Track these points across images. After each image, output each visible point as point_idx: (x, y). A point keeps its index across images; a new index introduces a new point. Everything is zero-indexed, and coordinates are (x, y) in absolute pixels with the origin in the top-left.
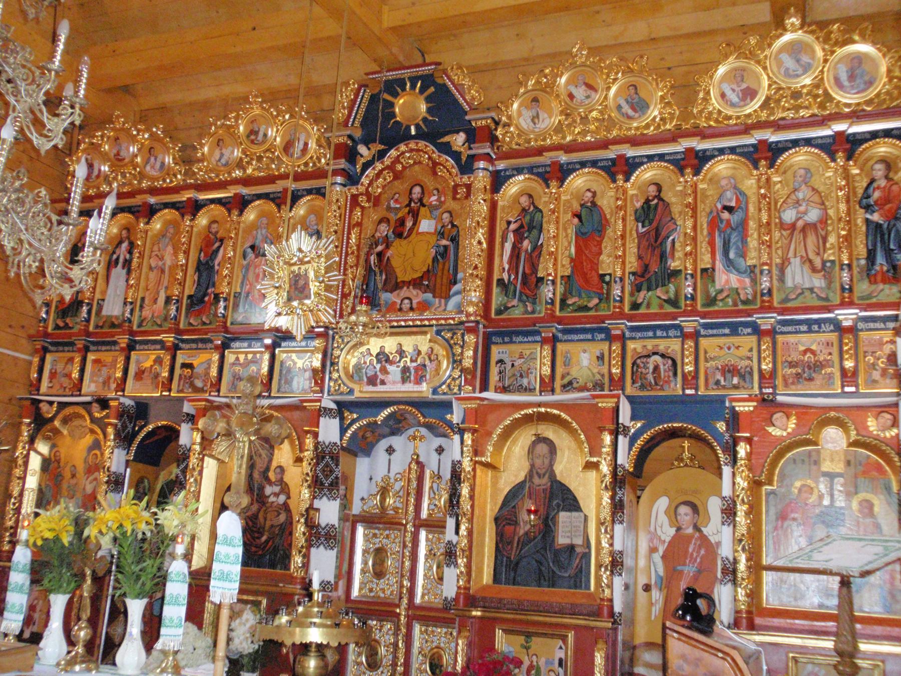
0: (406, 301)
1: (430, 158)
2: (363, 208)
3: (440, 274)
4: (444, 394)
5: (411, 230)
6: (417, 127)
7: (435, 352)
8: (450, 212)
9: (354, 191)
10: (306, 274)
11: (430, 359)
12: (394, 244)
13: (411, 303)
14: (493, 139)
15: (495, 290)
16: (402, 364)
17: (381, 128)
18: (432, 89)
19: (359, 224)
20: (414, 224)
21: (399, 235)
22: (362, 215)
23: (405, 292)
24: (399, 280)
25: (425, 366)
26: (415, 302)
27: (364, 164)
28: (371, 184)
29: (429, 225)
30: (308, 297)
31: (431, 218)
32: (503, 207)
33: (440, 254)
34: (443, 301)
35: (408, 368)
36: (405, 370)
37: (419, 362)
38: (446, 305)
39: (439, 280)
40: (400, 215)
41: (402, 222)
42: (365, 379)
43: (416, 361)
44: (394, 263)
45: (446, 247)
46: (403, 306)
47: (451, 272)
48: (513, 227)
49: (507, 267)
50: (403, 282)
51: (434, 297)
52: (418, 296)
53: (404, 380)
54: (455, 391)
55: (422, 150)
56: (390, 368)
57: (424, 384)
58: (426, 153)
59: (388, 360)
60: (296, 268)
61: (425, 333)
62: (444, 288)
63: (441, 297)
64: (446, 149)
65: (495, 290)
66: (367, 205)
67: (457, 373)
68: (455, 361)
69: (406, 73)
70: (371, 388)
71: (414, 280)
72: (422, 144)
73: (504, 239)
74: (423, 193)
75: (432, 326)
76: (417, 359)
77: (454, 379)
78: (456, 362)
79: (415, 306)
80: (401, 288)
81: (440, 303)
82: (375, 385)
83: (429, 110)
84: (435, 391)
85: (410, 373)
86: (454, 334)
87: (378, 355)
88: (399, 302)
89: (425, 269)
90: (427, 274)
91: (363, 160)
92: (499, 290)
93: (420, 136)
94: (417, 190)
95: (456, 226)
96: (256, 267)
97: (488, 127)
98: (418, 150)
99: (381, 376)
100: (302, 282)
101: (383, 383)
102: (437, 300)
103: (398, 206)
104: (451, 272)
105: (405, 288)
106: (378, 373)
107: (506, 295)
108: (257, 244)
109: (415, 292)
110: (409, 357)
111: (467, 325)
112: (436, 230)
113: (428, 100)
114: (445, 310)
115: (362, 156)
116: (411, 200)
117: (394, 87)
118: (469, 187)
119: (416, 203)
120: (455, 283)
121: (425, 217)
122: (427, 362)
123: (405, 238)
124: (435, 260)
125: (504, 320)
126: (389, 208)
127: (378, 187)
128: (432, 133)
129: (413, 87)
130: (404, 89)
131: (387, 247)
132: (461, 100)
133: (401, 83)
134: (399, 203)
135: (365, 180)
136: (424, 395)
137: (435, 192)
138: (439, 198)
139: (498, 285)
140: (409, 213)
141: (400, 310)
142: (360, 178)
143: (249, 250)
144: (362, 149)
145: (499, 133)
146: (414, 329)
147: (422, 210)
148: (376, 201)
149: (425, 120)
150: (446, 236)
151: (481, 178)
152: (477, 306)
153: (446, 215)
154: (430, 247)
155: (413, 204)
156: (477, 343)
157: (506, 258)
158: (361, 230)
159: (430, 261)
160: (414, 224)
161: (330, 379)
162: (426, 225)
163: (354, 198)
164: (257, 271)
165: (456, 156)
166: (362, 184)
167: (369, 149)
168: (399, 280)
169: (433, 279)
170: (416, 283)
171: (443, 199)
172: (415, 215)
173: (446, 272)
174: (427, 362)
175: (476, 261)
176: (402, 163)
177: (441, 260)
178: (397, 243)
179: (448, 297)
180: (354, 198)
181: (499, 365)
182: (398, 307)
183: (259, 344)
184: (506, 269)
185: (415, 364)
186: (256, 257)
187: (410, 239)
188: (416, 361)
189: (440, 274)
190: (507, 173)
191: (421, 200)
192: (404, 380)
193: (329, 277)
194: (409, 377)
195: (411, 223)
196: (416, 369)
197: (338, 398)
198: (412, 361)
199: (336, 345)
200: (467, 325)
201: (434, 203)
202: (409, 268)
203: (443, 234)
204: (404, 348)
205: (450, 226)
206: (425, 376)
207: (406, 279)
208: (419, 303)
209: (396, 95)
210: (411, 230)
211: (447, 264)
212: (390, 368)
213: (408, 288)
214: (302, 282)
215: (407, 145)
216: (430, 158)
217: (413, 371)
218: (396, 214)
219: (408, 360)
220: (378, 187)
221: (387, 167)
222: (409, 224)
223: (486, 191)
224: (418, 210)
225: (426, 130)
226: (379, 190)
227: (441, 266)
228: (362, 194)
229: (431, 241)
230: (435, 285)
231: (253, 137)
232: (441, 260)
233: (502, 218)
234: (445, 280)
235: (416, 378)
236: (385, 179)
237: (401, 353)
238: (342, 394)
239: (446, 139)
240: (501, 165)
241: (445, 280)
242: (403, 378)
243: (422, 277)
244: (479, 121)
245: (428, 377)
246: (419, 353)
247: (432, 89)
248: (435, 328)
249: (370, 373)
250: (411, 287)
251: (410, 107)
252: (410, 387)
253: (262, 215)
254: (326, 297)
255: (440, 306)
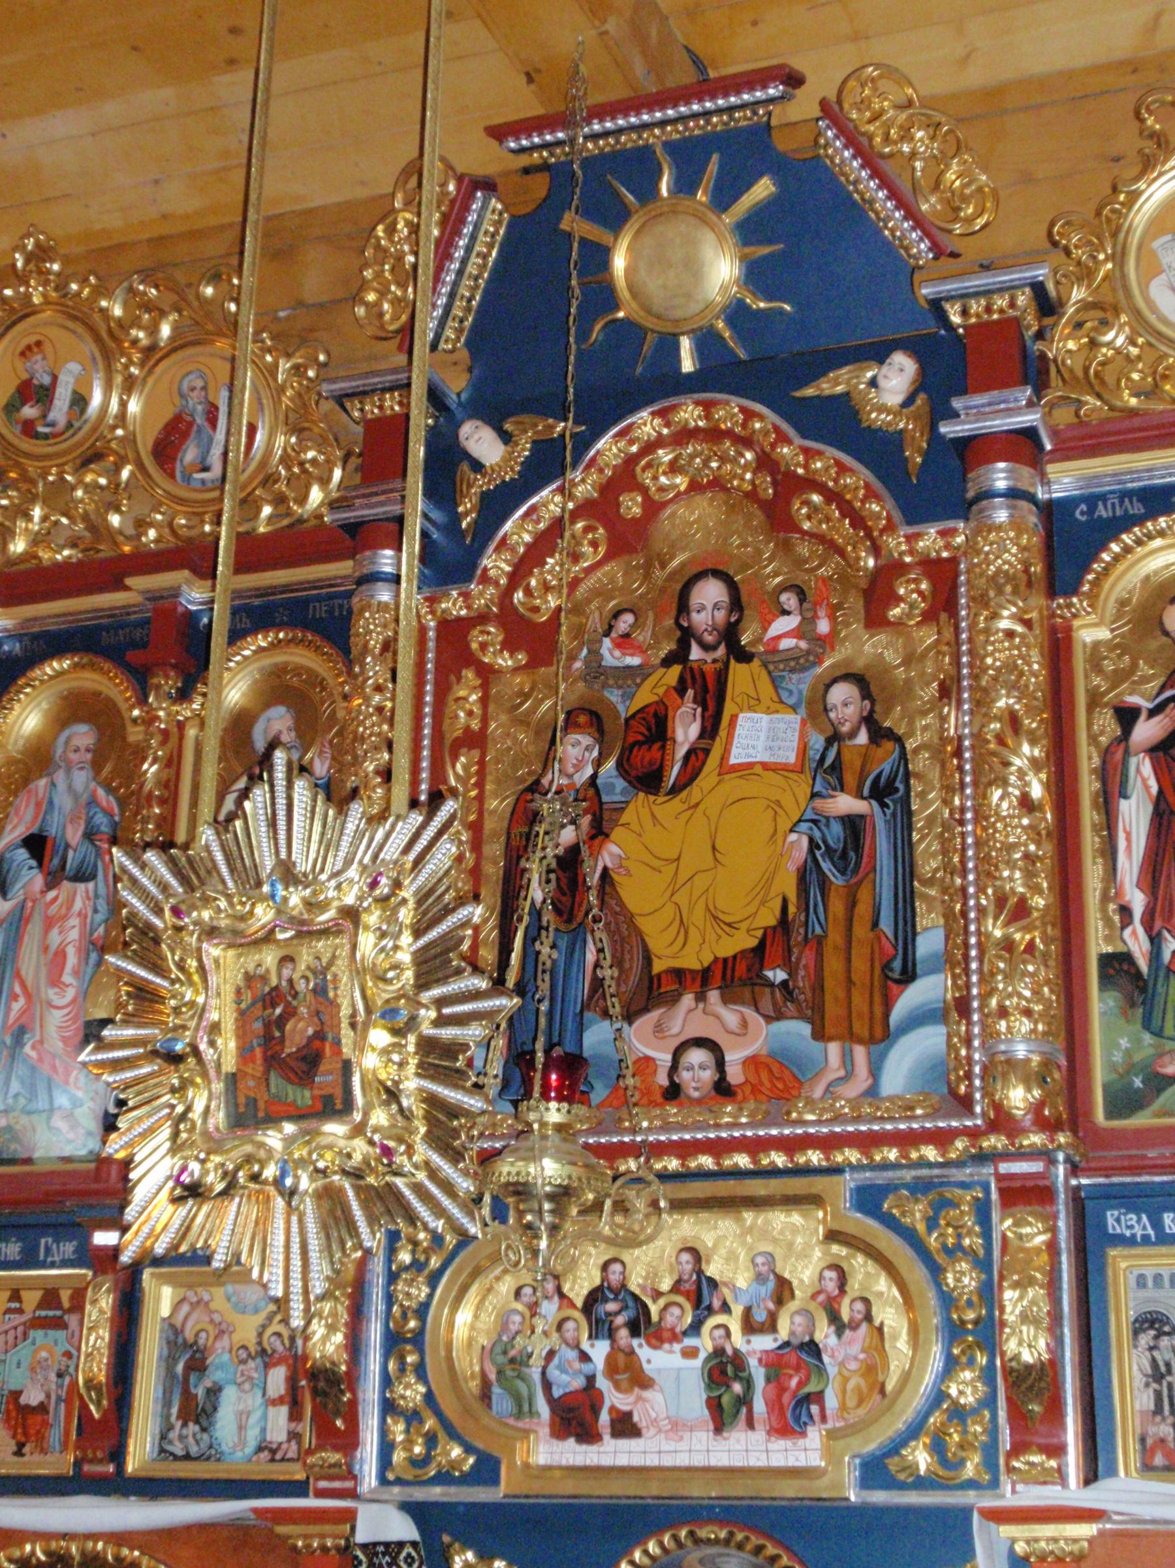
0: (696, 1056)
1: (766, 462)
2: (487, 673)
3: (835, 937)
4: (921, 1483)
5: (696, 756)
6: (706, 341)
7: (855, 1286)
8: (860, 680)
9: (453, 605)
10: (320, 991)
11: (834, 1318)
12: (627, 816)
13: (720, 1064)
14: (1036, 373)
15: (1100, 1004)
16: (705, 1343)
17: (553, 348)
18: (763, 189)
19: (475, 740)
20: (710, 730)
21: (648, 781)
22: (484, 701)
23: (685, 1016)
24: (658, 967)
25: (812, 1348)
26: (734, 1057)
27: (485, 496)
28: (517, 577)
29: (773, 735)
30: (337, 1105)
31: (780, 703)
32: (1095, 653)
33: (829, 851)
34: (860, 1052)
35: (738, 1361)
36: (723, 1369)
37: (783, 1334)
38: (875, 1072)
39: (833, 965)
40: (645, 696)
41: (655, 726)
42: (543, 1409)
43: (770, 1326)
44: (631, 894)
45: (854, 825)
46: (685, 1076)
47: (886, 925)
48: (1146, 731)
49: (1138, 901)
50: (679, 974)
51: (819, 1035)
52: (748, 1035)
53: (721, 1417)
54: (970, 1470)
55: (729, 433)
56: (656, 1360)
57: (814, 1436)
58: (746, 442)
59: (639, 1324)
60: (269, 958)
61: (816, 1200)
62: (859, 1000)
63: (851, 1037)
64: (839, 423)
65: (1100, 1004)
66: (505, 661)
67: (965, 1388)
68: (954, 1331)
69: (656, 127)
70: (571, 1453)
71: (726, 965)
72: (730, 411)
73: (1112, 790)
74: (736, 603)
75: (837, 1170)
76: (773, 1318)
77: (959, 1414)
78: (972, 1332)
79: (735, 1075)
80: (673, 999)
81: (847, 1060)
82: (588, 1435)
83: (755, 275)
84: (875, 1471)
85: (749, 1384)
86: (944, 1203)
87: (595, 1297)
88: (664, 1058)
89: (769, 917)
90: (778, 939)
91: (481, 484)
92: (1113, 999)
93: (719, 374)
94: (710, 593)
95: (890, 735)
96: (49, 923)
97: (1012, 325)
98: (714, 434)
99: (614, 1398)
100: (299, 1031)
101: (625, 1426)
102: (834, 1048)
103: (635, 661)
104: (886, 925)
105: (688, 1000)
106: (602, 1383)
107: (1147, 1024)
108: (52, 831)
109: (730, 1016)
110: (738, 1310)
111: (1005, 1168)
112: (803, 750)
113: (750, 230)
114: (872, 1092)
115: (477, 466)
116: (686, 636)
117: (613, 186)
118: (943, 573)
119: (706, 647)
120: (909, 976)
121: (754, 704)
122: (824, 1333)
123: (675, 790)
124: (809, 875)
125: (1143, 1137)
126: (596, 672)
127: (546, 588)
128: (764, 363)
129: (685, 185)
130: (648, 193)
131: (599, 832)
132: (896, 223)
133: (638, 167)
134: (640, 650)
135: (495, 564)
136: (821, 1488)
137: (789, 600)
138: (809, 621)
139: (1106, 980)
140: (681, 689)
141: (673, 1092)
142: (477, 552)
143: (22, 854)
144: (481, 442)
145: (1065, 345)
146: (758, 1188)
147: (739, 673)
148: (535, 640)
149: (737, 313)
150: (850, 779)
151: (1004, 541)
152: (1042, 1081)
153: (841, 693)
154: (785, 824)
155: (696, 653)
156: (1052, 1247)
157: (1130, 864)
158: (482, 763)
159: (788, 885)
160: (710, 730)
161: (389, 1407)
162: (761, 734)
163: (453, 633)
164: (55, 938)
165: (878, 450)
166: (485, 579)
167: (506, 438)
168: (658, 967)
169: (808, 958)
170: (735, 977)
171: (823, 627)
172: (712, 697)
173: (861, 931)
174: (824, 1333)
175: (1015, 881)
176: (644, 490)
177: (837, 880)
178: (640, 807)
179: (881, 1035)
180: (453, 633)
181: (1146, 1339)
182: (662, 1080)
183: (68, 1248)
184: (1138, 910)
185: (765, 1342)
186: (52, 881)
187: (695, 792)
188: (770, 1326)
189: (835, 937)
190: (1102, 512)
191: (730, 634)
192: (721, 1417)
193: (440, 1002)
194: (745, 1401)
195: (694, 730)
196: (775, 1363)
197: (419, 1494)
198: (750, 1327)
199: (405, 1257)
200: (1005, 1168)
201: (786, 644)
202: (698, 916)
203: (836, 768)
204: (711, 1270)
205: (863, 738)
206: (819, 1397)
207: (692, 961)
208: (752, 1062)
209: (616, 218)
210: (696, 756)
211: (864, 895)
212: (656, 1360)
213: (701, 997)
214: (299, 1031)
215: (708, 406)
216: (766, 462)
217: (759, 1375)
218: (629, 697)
219: (734, 1324)
220: (546, 588)
221: (585, 509)
222: (686, 731)
223: (1029, 584)
224: (722, 677)
225: (742, 354)
226: (553, 602)
227: (837, 906)
228: (482, 618)
229: (787, 801)
230: (818, 986)
231: (29, 411)
232: (837, 880)
233: (1094, 700)
234: (860, 965)
235: (776, 1405)
236: (576, 557)
237: (700, 1293)
238: (443, 1478)
239: (834, 384)
240: (1064, 480)
241: (860, 965)
242: (715, 1406)
243: (760, 950)
244: (969, 302)
245: (831, 1401)
246: (783, 1290)
247: (763, 189)
248: (849, 1180)
249: (567, 1382)
250: (714, 996)
251: (692, 268)
252: (750, 1449)
253: (75, 708)
254: (432, 1101)
255: (849, 1075)
